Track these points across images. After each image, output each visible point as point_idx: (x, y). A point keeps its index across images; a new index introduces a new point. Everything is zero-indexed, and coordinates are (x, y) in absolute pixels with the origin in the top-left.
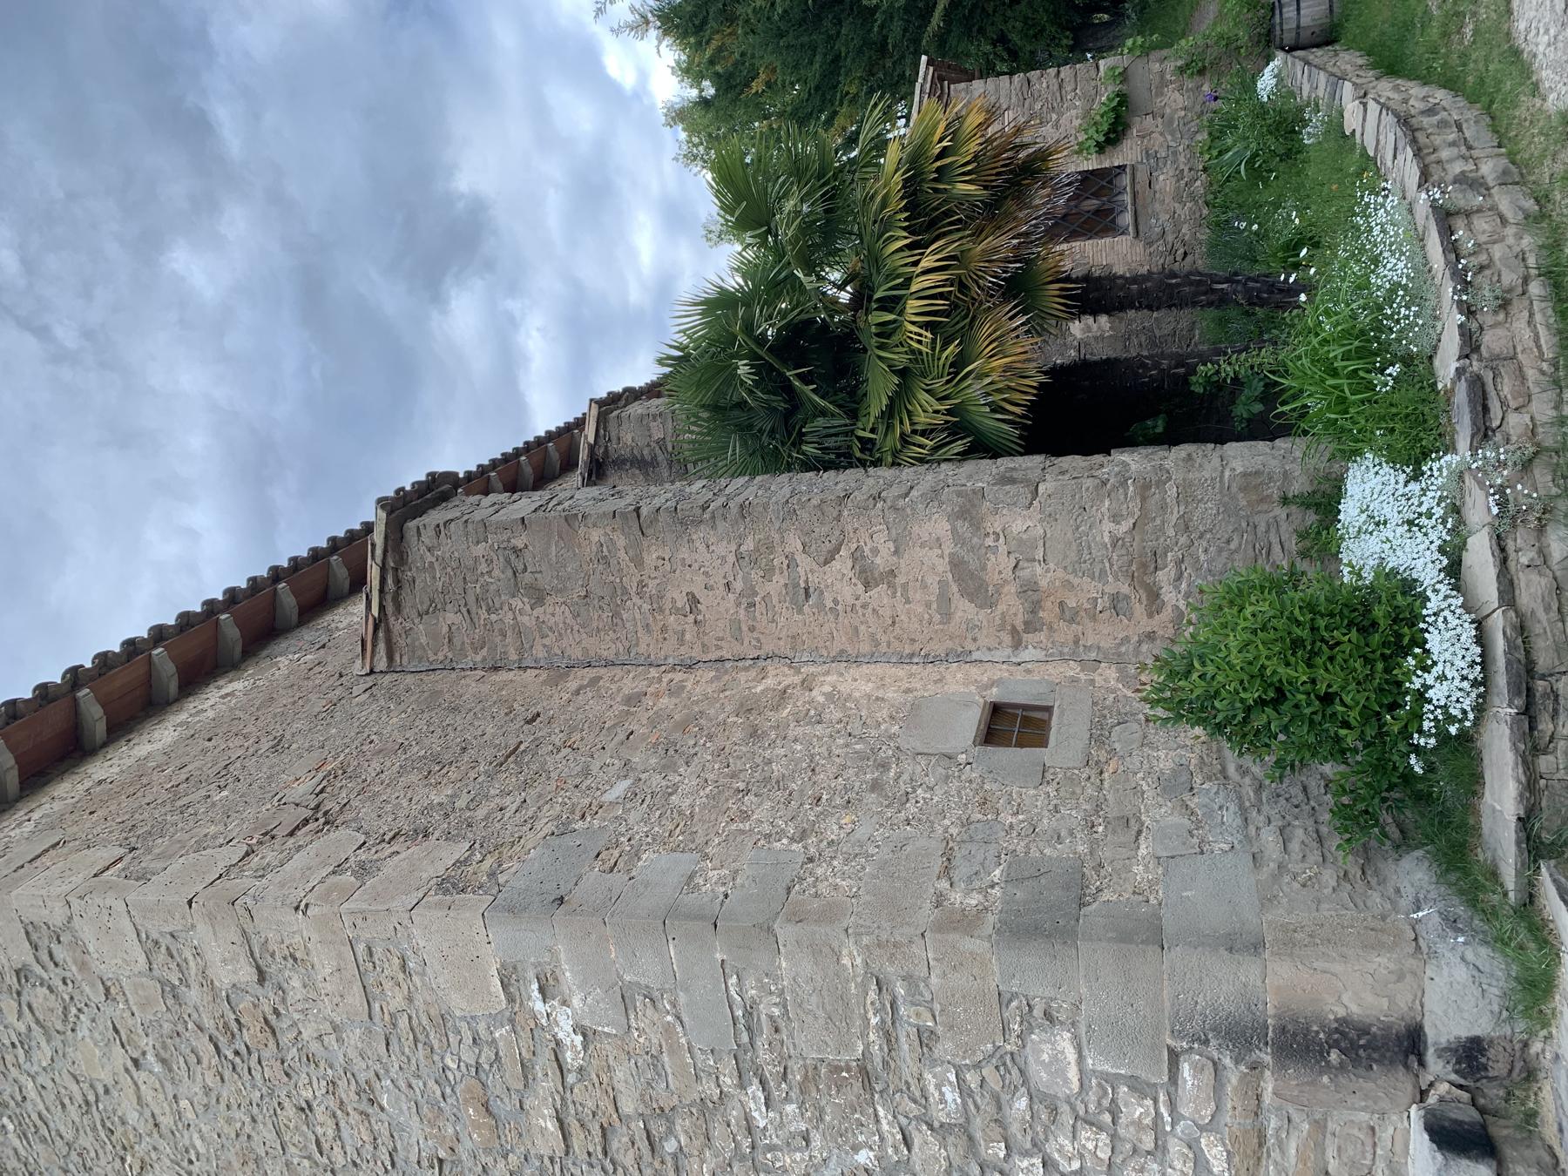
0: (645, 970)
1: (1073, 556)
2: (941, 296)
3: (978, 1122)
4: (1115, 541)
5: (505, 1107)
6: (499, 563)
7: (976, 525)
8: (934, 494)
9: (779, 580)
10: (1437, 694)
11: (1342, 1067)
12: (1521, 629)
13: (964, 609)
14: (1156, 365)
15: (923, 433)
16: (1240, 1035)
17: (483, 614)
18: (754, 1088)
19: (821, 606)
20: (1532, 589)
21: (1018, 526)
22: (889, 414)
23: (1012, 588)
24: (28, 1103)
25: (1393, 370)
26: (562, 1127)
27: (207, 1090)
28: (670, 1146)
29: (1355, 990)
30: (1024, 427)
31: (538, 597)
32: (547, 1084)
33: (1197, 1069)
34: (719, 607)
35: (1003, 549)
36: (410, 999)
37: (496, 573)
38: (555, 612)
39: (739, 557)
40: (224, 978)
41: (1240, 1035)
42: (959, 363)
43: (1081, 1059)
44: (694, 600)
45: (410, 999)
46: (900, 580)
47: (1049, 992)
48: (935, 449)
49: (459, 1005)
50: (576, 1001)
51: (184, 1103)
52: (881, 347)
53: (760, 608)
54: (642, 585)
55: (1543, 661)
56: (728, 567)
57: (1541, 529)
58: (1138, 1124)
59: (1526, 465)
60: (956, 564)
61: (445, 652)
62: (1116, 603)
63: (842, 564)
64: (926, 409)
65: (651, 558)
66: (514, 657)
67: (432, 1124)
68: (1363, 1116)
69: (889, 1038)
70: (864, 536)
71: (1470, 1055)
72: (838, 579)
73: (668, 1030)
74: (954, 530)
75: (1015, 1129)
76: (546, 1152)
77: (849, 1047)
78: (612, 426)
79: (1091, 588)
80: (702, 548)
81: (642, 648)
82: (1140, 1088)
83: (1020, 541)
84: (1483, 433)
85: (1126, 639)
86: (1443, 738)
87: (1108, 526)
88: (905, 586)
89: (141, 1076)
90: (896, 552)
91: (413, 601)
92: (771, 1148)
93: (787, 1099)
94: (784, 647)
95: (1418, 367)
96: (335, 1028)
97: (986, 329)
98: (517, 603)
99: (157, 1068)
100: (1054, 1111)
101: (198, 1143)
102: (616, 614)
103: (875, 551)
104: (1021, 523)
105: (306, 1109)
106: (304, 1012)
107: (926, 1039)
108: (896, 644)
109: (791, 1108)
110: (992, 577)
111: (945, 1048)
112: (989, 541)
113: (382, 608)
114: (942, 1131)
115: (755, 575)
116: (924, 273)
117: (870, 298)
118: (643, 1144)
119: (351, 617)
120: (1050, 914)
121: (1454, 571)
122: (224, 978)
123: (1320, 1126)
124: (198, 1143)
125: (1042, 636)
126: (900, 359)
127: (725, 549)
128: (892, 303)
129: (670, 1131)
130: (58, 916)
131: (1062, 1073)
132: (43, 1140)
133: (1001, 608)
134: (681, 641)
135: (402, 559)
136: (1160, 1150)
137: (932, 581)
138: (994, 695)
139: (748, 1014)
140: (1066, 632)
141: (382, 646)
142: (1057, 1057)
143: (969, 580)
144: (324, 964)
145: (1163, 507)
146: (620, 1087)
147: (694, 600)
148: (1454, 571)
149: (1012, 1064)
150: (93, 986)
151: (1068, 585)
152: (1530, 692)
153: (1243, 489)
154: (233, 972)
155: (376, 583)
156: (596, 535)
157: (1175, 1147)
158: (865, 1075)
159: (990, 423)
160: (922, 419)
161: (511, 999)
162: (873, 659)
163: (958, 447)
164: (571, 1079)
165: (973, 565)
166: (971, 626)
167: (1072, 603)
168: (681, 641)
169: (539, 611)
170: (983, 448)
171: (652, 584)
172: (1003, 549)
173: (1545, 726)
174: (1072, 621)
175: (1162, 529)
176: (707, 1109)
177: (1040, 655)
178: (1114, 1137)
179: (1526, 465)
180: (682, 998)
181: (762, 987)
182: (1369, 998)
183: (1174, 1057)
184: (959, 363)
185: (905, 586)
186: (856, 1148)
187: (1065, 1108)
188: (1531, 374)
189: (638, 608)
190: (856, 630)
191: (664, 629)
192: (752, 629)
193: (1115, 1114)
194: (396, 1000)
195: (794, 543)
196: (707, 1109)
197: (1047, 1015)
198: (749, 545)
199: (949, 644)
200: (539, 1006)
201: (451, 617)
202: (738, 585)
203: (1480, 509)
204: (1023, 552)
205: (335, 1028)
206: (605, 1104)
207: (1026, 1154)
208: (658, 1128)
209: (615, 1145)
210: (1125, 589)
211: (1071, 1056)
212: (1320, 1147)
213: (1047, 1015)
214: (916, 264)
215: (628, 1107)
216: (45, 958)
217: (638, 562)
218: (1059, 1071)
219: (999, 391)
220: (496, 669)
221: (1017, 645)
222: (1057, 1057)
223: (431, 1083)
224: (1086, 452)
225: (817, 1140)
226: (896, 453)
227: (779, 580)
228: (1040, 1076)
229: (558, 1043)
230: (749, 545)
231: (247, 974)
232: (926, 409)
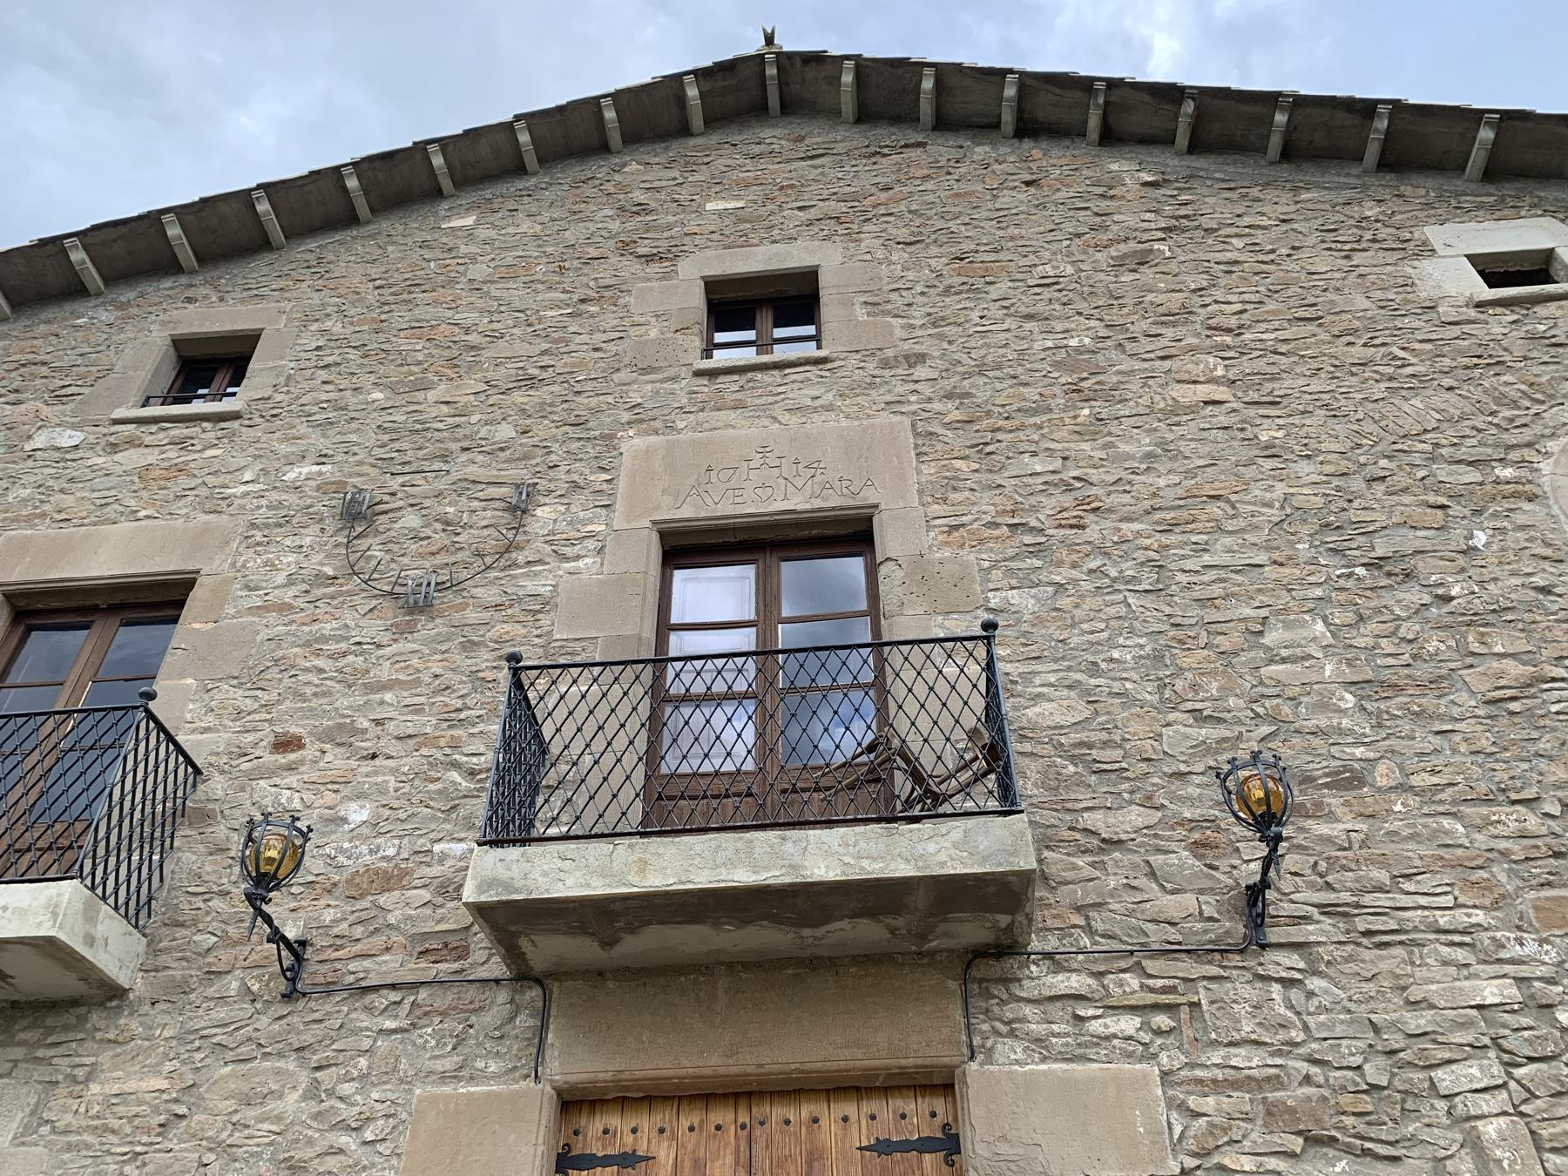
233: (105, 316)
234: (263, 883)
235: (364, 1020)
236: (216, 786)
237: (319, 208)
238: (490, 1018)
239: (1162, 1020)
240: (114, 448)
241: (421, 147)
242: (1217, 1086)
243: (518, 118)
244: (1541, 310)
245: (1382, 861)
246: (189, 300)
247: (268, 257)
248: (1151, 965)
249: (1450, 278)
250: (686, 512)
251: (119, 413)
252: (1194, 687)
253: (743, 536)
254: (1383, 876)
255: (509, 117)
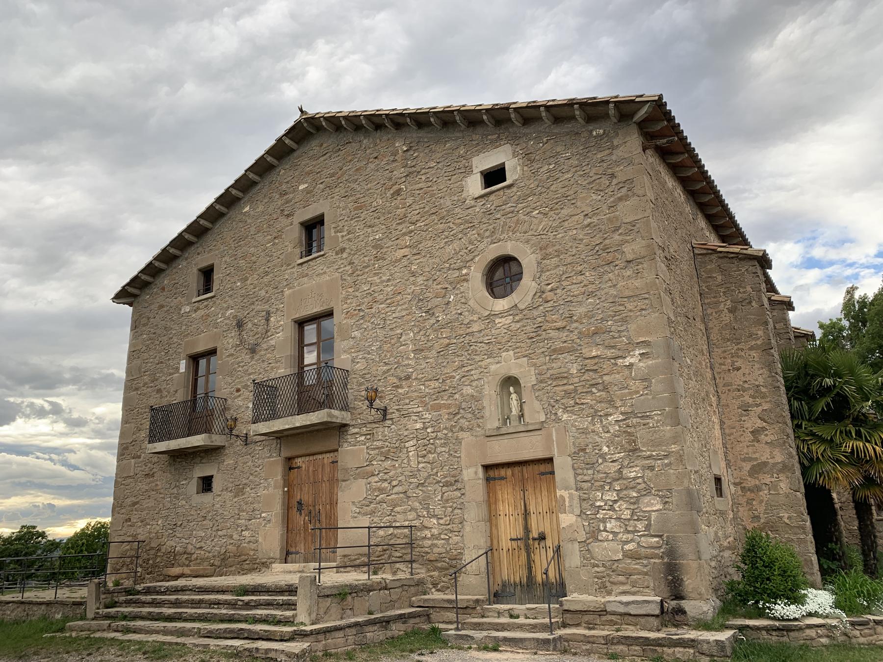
0: (656, 384)
1: (773, 503)
2: (865, 456)
3: (625, 482)
4: (781, 518)
5: (598, 339)
6: (745, 296)
7: (781, 471)
8: (790, 456)
9: (751, 401)
10: (777, 607)
11: (667, 580)
12: (800, 629)
13: (747, 466)
14: (836, 531)
15: (808, 448)
16: (671, 553)
17: (722, 290)
18: (621, 417)
19: (742, 415)
20: (812, 633)
21: (782, 485)
22: (813, 434)
23: (757, 482)
24: (561, 174)
25: (865, 603)
26: (594, 357)
27: (581, 240)
28: (594, 390)
29: (690, 583)
30: (814, 484)
31: (732, 311)
32: (609, 353)
33: (658, 542)
34: (737, 378)
35: (773, 480)
36: (631, 311)
37: (740, 295)
38: (727, 317)
39: (758, 386)
40: (627, 248)
41: (671, 553)
42: (838, 461)
43: (654, 511)
44: (738, 369)
45: (631, 311)
46: (756, 444)
47: (674, 503)
48: (803, 453)
49: (632, 327)
50: (641, 364)
51: (575, 232)
52: (841, 432)
53: (738, 393)
54: (742, 350)
55: (791, 634)
56: (753, 382)
57: (828, 636)
58: (636, 526)
59: (846, 634)
60: (765, 464)
61: (705, 275)
62: (756, 518)
63: (759, 424)
64: (818, 449)
65: (753, 353)
66: (706, 301)
67: (585, 315)
68: (652, 585)
69: (649, 457)
70: (773, 431)
71: (681, 611)
72: (753, 422)
73: (638, 392)
74: (778, 463)
75: (625, 492)
76: (583, 351)
77: (644, 446)
78: (780, 306)
79: (761, 509)
80: (760, 372)
81: (716, 350)
82: (648, 527)
83: (777, 486)
84: (853, 624)
85: (743, 521)
86: (764, 609)
87: (786, 515)
88: (754, 446)
89: (581, 216)
90: (767, 443)
91: (725, 264)
92: (601, 421)
93: (620, 427)
94: (723, 402)
95: (867, 610)
96: (615, 286)
97: (851, 470)
98: (729, 302)
99: (586, 222)
100: (634, 503)
101: (560, 235)
102: (728, 340)
103: (766, 435)
104: (784, 486)
105: (581, 273)
106: (619, 275)
107: (651, 468)
108: (730, 442)
109: (617, 428)
110: (761, 476)
111: (648, 473)
112: (775, 475)
113: (721, 252)
114: (620, 471)
115: (751, 392)
116: (874, 449)
117: (861, 426)
118: (593, 382)
119: (713, 241)
120: (691, 501)
121: (810, 615)
122: (627, 248)
123: (646, 574)
124: (560, 235)
125: (740, 493)
126: (838, 439)
127: (761, 381)
128: (859, 434)
129: (599, 391)
130: (638, 190)
131: (648, 506)
132: (548, 179)
133: (749, 479)
134: (721, 364)
135: (741, 259)
136: (629, 532)
137: (757, 455)
138: (723, 478)
139: (647, 416)
140: (743, 500)
141: (705, 252)
142: (653, 505)
143: (759, 468)
144: (638, 283)
145: (796, 534)
146: (613, 376)
147: (738, 369)
148: (810, 615)
149: (648, 491)
150: (613, 202)
151: (761, 501)
152: (783, 630)
153: (805, 560)
154: (629, 251)
155: (731, 250)
156: (760, 333)
157: (630, 536)
158: (635, 450)
159: (815, 472)
160: (814, 448)
161: (637, 343)
162: (723, 434)
163: (806, 462)
164: (613, 361)
165: (765, 470)
166: (741, 469)
167: (754, 503)
168: (721, 364)
169: (726, 311)
170: (805, 471)
171: (743, 354)
172: (773, 480)
173: (774, 633)
174: (747, 503)
175: (787, 533)
176: (611, 402)
177: (733, 492)
178: (629, 520)
179: (846, 634)
180: (650, 397)
181: (658, 421)
182: (691, 586)
183: (660, 536)
184: (838, 461)
185: (754, 446)
186: (608, 446)
187: (636, 506)
188: (871, 638)
189: (732, 347)
190: (734, 428)
191: (725, 358)
192: (729, 390)
193: (638, 520)
194: (630, 306)
195: (766, 406)
196: (611, 402)
197: (666, 502)
198: (763, 390)
199: (732, 461)
200: (637, 352)
201: (719, 278)
202: (746, 386)
203: (834, 622)
204: (773, 487)
205: (615, 286)
206: (606, 372)
207: (618, 495)
208: (600, 387)
209: (591, 373)
210: (762, 521)
211: (654, 509)
212: (639, 574)
213: (666, 502)
214: (876, 444)
215: (605, 378)
216: (621, 185)
217: (751, 348)
218: (649, 504)
219: (828, 476)
220: (701, 295)
221: (735, 484)
222: (653, 505)
223: (601, 316)
224: (809, 507)
225: (607, 435)
226: (799, 437)
227: (751, 401)
228: (646, 500)
229: (625, 358)
230: (763, 390)
231: (630, 257)
232: (818, 449)
233: (184, 263)
234: (371, 401)
235: (257, 448)
236: (229, 402)
237: (213, 216)
238: (273, 446)
239: (368, 437)
240: (196, 311)
241: (227, 190)
242: (374, 449)
243: (246, 171)
244: (492, 197)
245: (407, 398)
246: (198, 254)
247: (210, 232)
248: (368, 426)
249: (474, 185)
250: (297, 316)
251: (194, 300)
252: (386, 356)
253: (49, 491)
254: (407, 401)
255: (243, 172)
